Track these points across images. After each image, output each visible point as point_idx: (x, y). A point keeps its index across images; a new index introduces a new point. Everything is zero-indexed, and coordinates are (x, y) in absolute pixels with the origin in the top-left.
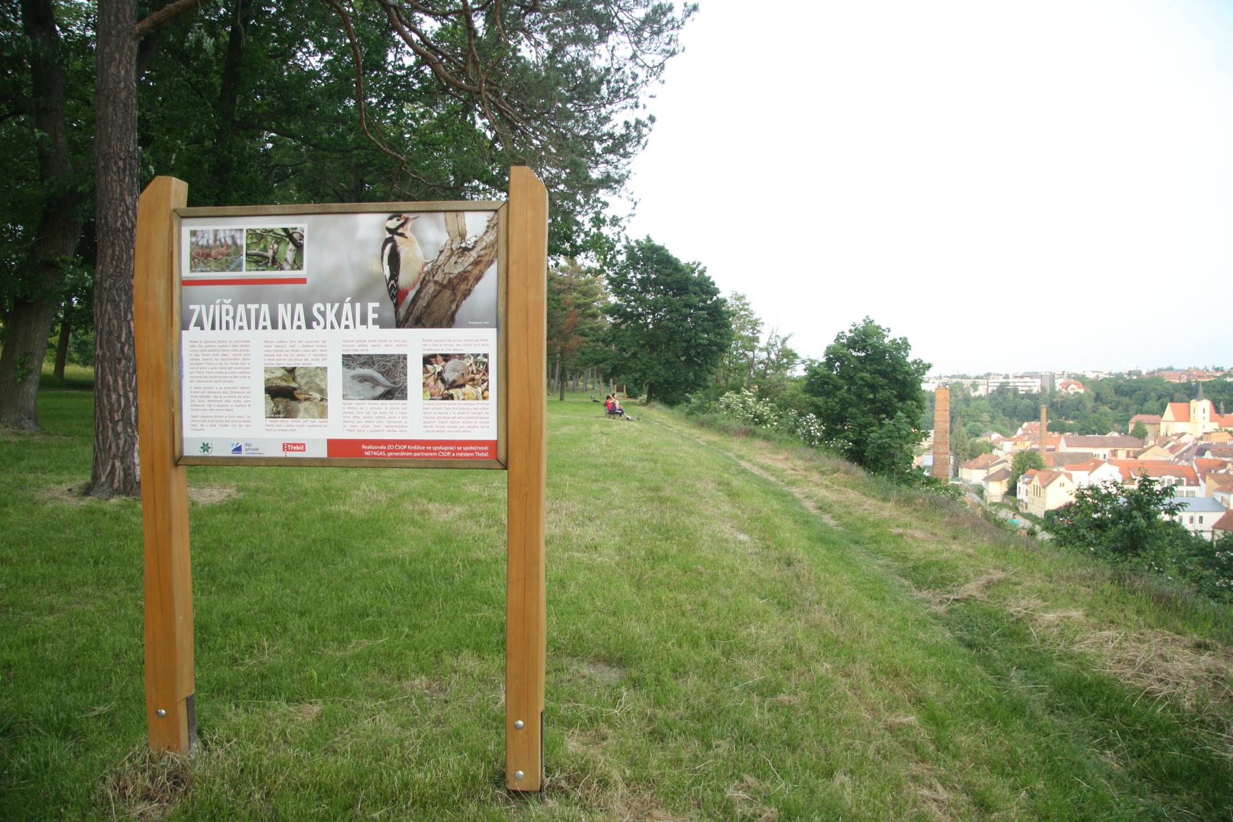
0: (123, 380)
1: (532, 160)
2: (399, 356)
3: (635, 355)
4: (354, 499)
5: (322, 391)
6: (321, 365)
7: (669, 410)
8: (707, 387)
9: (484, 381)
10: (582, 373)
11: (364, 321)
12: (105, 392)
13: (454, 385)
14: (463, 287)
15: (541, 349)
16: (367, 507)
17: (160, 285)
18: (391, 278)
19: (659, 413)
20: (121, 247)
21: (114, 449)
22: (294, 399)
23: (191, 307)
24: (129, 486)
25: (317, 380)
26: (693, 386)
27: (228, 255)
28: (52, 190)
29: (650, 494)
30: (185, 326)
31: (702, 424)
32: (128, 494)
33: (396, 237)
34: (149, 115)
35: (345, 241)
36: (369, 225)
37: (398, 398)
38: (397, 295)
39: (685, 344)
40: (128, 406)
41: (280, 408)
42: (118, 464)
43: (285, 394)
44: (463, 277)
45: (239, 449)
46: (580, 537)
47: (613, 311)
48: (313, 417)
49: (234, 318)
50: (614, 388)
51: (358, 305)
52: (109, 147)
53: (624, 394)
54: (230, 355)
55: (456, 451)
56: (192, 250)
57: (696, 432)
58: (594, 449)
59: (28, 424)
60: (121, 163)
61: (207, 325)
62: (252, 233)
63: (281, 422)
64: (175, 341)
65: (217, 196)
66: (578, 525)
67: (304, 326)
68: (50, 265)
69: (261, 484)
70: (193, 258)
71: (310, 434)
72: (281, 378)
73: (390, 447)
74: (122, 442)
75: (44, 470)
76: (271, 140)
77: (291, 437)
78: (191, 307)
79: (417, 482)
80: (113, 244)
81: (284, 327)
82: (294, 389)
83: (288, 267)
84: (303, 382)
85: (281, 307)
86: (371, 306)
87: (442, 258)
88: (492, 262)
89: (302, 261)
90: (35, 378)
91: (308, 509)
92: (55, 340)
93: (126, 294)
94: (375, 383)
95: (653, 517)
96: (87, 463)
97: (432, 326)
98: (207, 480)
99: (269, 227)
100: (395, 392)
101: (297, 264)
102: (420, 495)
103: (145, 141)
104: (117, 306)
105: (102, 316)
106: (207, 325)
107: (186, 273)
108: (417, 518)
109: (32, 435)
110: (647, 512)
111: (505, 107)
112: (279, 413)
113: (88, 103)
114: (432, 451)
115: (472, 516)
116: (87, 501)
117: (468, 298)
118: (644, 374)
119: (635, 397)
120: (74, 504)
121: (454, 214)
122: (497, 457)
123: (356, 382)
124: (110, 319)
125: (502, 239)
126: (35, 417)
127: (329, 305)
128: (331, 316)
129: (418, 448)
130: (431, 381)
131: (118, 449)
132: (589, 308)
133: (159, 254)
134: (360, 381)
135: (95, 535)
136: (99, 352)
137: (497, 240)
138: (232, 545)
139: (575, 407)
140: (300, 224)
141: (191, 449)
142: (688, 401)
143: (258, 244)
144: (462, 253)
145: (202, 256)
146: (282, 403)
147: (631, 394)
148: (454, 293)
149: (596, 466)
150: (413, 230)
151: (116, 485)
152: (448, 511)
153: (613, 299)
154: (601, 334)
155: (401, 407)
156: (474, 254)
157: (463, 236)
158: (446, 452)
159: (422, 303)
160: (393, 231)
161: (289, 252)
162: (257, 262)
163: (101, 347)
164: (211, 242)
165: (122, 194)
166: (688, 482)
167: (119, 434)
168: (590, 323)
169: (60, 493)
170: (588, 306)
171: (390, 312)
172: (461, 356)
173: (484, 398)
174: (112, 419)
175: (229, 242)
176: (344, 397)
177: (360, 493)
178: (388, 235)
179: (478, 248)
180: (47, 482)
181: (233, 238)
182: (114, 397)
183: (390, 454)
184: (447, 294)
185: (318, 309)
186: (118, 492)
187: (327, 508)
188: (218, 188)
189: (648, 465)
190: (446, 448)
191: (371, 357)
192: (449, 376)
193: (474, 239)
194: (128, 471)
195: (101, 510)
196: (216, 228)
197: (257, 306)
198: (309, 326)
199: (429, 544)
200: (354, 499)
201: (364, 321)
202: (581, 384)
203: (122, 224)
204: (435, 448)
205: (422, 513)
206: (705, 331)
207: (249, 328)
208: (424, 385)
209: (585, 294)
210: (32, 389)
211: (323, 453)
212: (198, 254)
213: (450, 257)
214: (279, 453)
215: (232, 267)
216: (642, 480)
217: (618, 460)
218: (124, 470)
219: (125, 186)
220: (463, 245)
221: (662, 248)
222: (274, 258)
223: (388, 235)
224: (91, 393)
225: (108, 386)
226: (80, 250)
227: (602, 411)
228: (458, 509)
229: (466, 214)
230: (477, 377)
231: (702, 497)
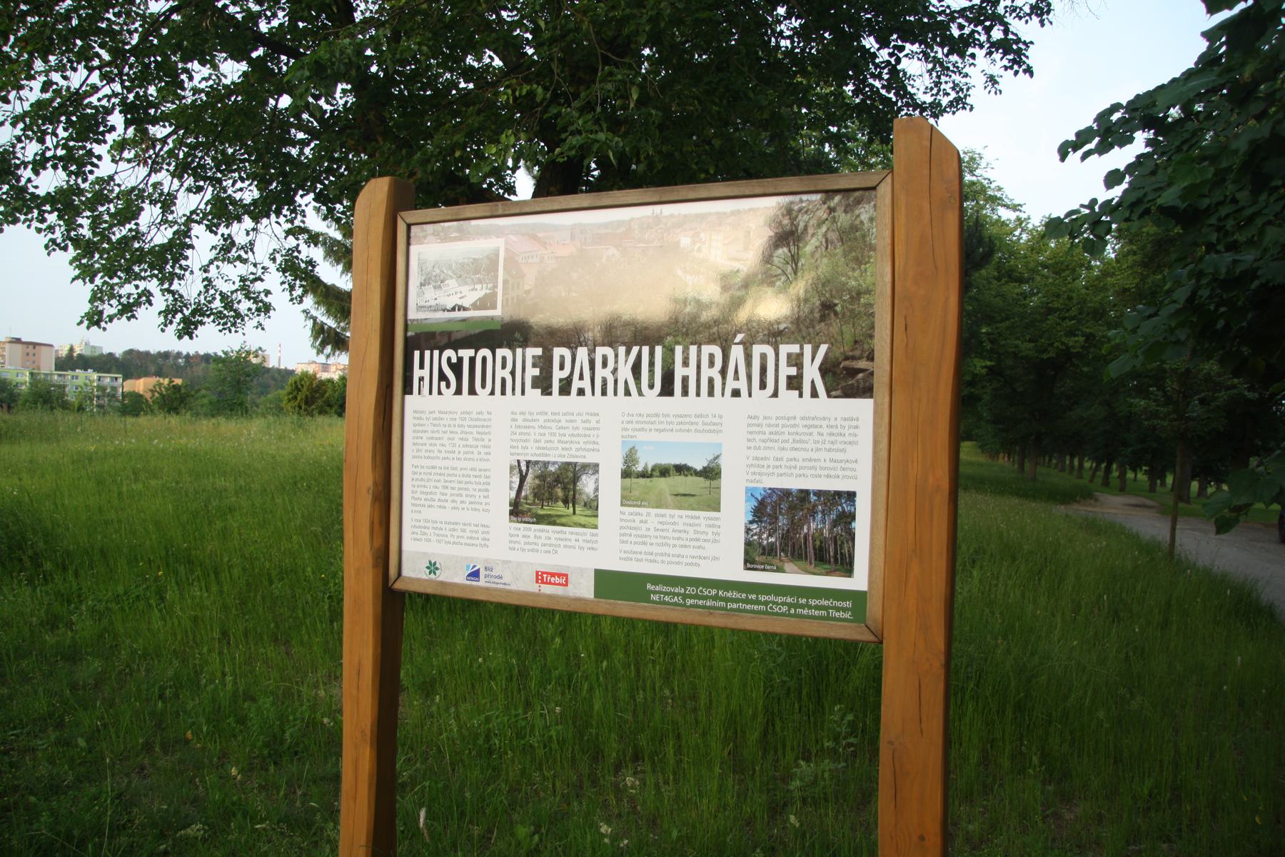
45: (475, 574)
49: (723, 372)
55: (797, 606)
77: (549, 562)
114: (757, 602)
129: (735, 595)
190: (780, 599)
197: (471, 352)
201: (795, 383)
204: (762, 598)
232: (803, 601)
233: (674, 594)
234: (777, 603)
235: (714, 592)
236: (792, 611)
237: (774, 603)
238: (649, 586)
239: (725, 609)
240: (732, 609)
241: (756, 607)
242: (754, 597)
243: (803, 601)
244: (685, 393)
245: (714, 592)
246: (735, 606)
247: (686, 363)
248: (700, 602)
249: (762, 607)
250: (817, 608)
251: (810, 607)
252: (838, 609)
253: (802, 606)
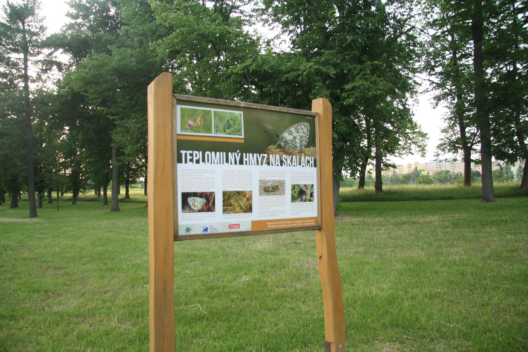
28: (101, 72)
45: (206, 229)
55: (303, 223)
73: (278, 223)
81: (272, 165)
114: (294, 223)
128: (289, 161)
129: (309, 221)
190: (299, 222)
197: (185, 152)
204: (296, 222)
214: (227, 230)
244: (246, 164)
247: (246, 157)
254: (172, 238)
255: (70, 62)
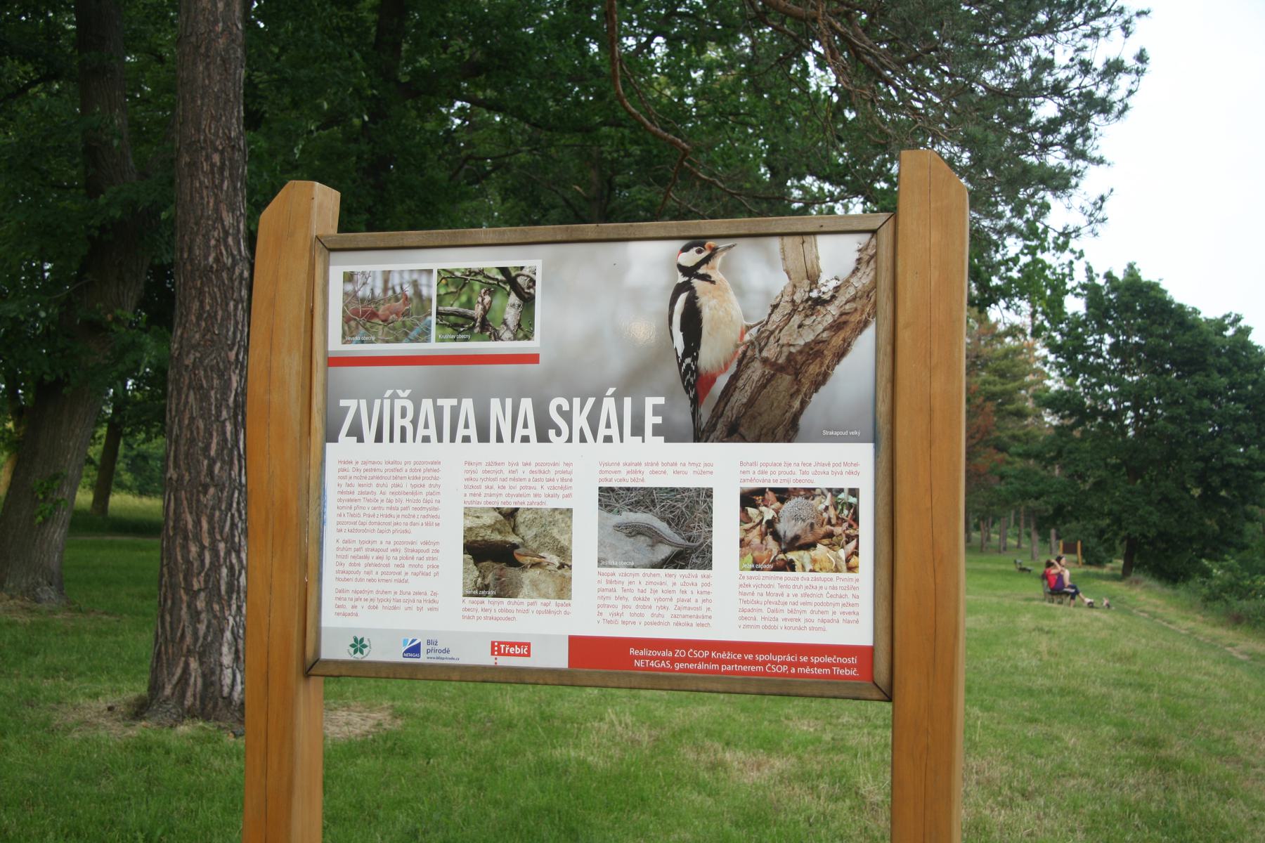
0: (211, 521)
1: (919, 131)
2: (698, 490)
3: (1099, 485)
4: (594, 738)
5: (563, 551)
6: (563, 504)
7: (1168, 591)
8: (1244, 547)
9: (850, 538)
10: (997, 518)
11: (638, 430)
12: (179, 541)
13: (796, 544)
14: (813, 369)
15: (957, 480)
16: (616, 752)
17: (291, 364)
18: (685, 355)
19: (1147, 596)
20: (214, 298)
21: (189, 639)
22: (515, 564)
23: (343, 403)
24: (212, 704)
25: (555, 532)
26: (1217, 546)
27: (406, 314)
29: (1140, 752)
30: (332, 437)
31: (1237, 620)
32: (207, 718)
33: (696, 283)
34: (260, 77)
35: (606, 290)
36: (649, 261)
37: (695, 567)
38: (695, 382)
39: (1200, 465)
40: (215, 567)
41: (490, 579)
42: (194, 664)
43: (499, 555)
44: (814, 351)
45: (415, 650)
46: (1008, 828)
47: (1056, 403)
48: (546, 596)
49: (415, 422)
50: (1058, 546)
51: (628, 401)
52: (198, 130)
53: (1078, 557)
54: (406, 486)
55: (798, 665)
56: (346, 305)
57: (1227, 635)
58: (1026, 659)
59: (48, 593)
60: (216, 158)
61: (369, 435)
62: (447, 277)
63: (490, 604)
64: (314, 460)
65: (369, 210)
66: (1003, 805)
67: (533, 437)
68: (95, 328)
69: (433, 706)
70: (347, 320)
71: (539, 626)
72: (493, 527)
73: (679, 653)
74: (202, 628)
75: (69, 672)
76: (461, 113)
78: (343, 403)
79: (704, 709)
80: (201, 292)
81: (500, 439)
82: (515, 546)
83: (508, 335)
84: (529, 534)
85: (495, 404)
86: (650, 402)
87: (776, 317)
88: (866, 324)
89: (532, 325)
90: (65, 515)
91: (515, 754)
92: (95, 451)
93: (221, 376)
94: (656, 538)
95: (1149, 798)
96: (140, 661)
97: (758, 441)
98: (341, 695)
99: (476, 265)
100: (690, 555)
101: (524, 329)
102: (709, 734)
103: (253, 121)
104: (205, 397)
105: (180, 413)
106: (369, 435)
107: (336, 345)
108: (705, 775)
109: (51, 612)
110: (1136, 787)
111: (864, 43)
112: (486, 587)
113: (161, 59)
114: (755, 663)
115: (804, 777)
116: (137, 730)
117: (823, 389)
118: (1118, 520)
119: (1099, 563)
120: (115, 733)
121: (798, 239)
122: (871, 676)
123: (621, 536)
124: (192, 419)
125: (885, 283)
126: (58, 582)
127: (577, 401)
128: (580, 421)
129: (828, 660)
130: (754, 537)
131: (196, 639)
132: (1011, 400)
133: (291, 310)
134: (630, 535)
135: (149, 790)
136: (172, 473)
137: (875, 285)
138: (381, 814)
139: (985, 579)
140: (529, 260)
141: (334, 649)
142: (1206, 573)
143: (456, 295)
144: (813, 308)
145: (363, 316)
146: (493, 570)
147: (1092, 558)
148: (797, 380)
149: (1030, 692)
150: (725, 269)
151: (189, 701)
152: (759, 766)
153: (1055, 384)
154: (1035, 447)
155: (679, 580)
156: (833, 310)
157: (813, 279)
158: (779, 666)
159: (740, 398)
160: (688, 271)
161: (509, 308)
162: (454, 326)
163: (177, 466)
164: (378, 292)
165: (217, 210)
166: (1217, 732)
167: (198, 613)
168: (1012, 426)
169: (94, 713)
170: (1009, 397)
171: (683, 415)
172: (810, 493)
173: (851, 569)
174: (188, 588)
175: (409, 291)
176: (601, 562)
177: (605, 727)
178: (681, 279)
179: (841, 299)
180: (74, 694)
181: (415, 284)
182: (194, 549)
183: (679, 666)
184: (785, 380)
185: (559, 408)
186: (191, 714)
187: (546, 753)
188: (386, 202)
189: (1134, 696)
190: (779, 658)
191: (649, 491)
192: (788, 528)
193: (833, 284)
194: (210, 678)
195: (161, 745)
196: (387, 267)
197: (454, 402)
198: (543, 438)
199: (727, 825)
200: (594, 738)
201: (638, 430)
202: (995, 537)
203: (217, 260)
204: (760, 658)
205: (713, 767)
206: (1240, 440)
207: (440, 440)
208: (743, 543)
209: (1002, 375)
210: (58, 534)
211: (560, 660)
212: (356, 312)
213: (790, 316)
214: (484, 658)
215: (413, 334)
216: (1121, 725)
217: (1074, 683)
218: (204, 676)
219: (223, 196)
220: (814, 294)
221: (1153, 287)
222: (484, 319)
223: (681, 279)
224: (156, 541)
225: (185, 530)
226: (143, 304)
227: (1037, 588)
228: (778, 763)
229: (822, 241)
230: (838, 530)
231: (1248, 765)
232: (805, 659)
233: (661, 659)
234: (776, 663)
235: (706, 654)
236: (793, 670)
237: (772, 662)
238: (632, 651)
239: (719, 672)
240: (727, 672)
241: (753, 668)
242: (750, 657)
243: (805, 659)
245: (706, 654)
246: (730, 668)
248: (691, 666)
249: (760, 668)
250: (820, 665)
251: (812, 665)
252: (842, 666)
253: (804, 665)
254: (295, 665)
255: (1046, 230)
